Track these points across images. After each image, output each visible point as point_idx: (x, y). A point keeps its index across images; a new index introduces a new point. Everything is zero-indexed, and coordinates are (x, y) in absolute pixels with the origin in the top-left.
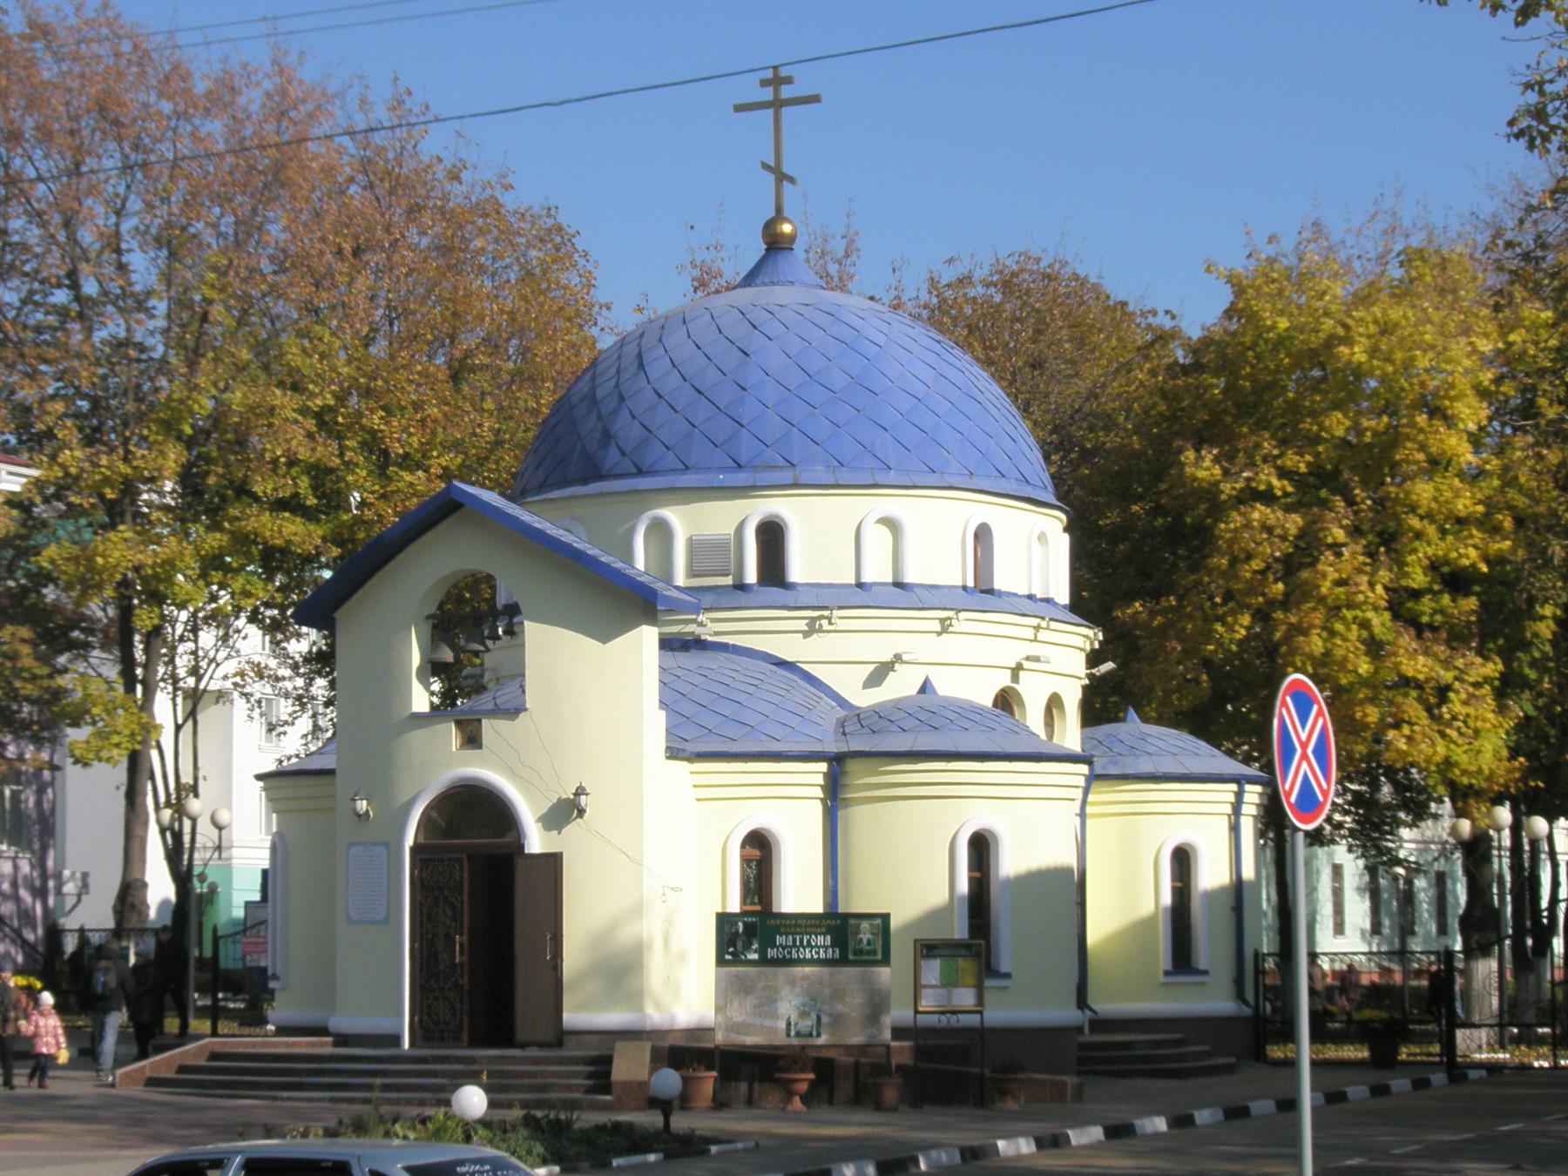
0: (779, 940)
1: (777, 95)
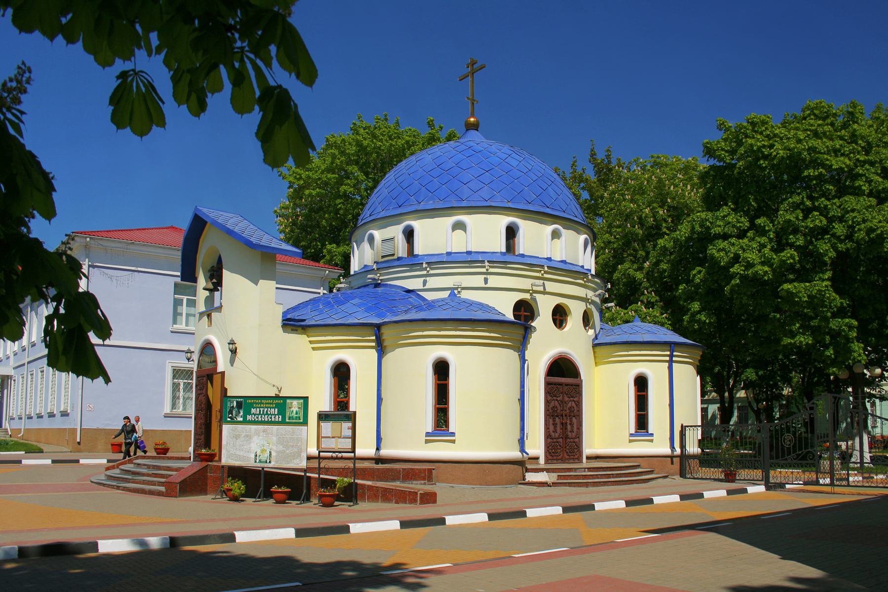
0: (253, 411)
1: (474, 68)
